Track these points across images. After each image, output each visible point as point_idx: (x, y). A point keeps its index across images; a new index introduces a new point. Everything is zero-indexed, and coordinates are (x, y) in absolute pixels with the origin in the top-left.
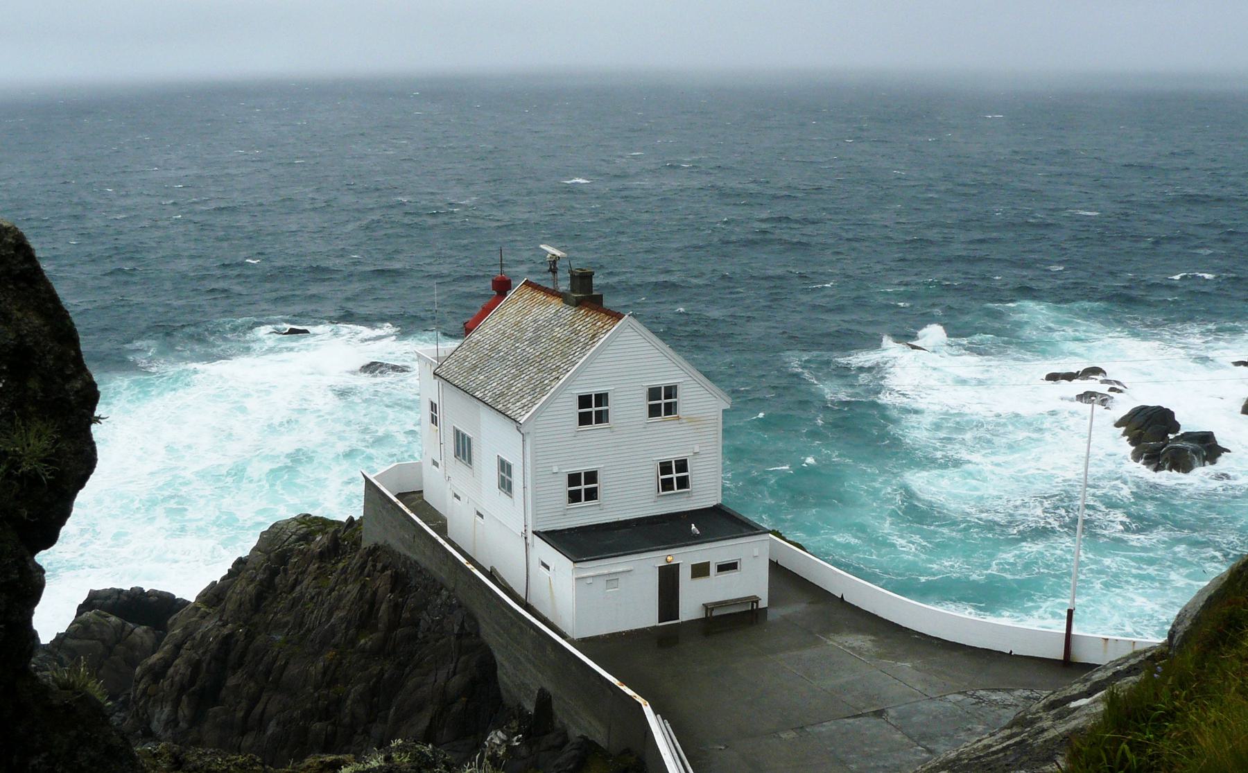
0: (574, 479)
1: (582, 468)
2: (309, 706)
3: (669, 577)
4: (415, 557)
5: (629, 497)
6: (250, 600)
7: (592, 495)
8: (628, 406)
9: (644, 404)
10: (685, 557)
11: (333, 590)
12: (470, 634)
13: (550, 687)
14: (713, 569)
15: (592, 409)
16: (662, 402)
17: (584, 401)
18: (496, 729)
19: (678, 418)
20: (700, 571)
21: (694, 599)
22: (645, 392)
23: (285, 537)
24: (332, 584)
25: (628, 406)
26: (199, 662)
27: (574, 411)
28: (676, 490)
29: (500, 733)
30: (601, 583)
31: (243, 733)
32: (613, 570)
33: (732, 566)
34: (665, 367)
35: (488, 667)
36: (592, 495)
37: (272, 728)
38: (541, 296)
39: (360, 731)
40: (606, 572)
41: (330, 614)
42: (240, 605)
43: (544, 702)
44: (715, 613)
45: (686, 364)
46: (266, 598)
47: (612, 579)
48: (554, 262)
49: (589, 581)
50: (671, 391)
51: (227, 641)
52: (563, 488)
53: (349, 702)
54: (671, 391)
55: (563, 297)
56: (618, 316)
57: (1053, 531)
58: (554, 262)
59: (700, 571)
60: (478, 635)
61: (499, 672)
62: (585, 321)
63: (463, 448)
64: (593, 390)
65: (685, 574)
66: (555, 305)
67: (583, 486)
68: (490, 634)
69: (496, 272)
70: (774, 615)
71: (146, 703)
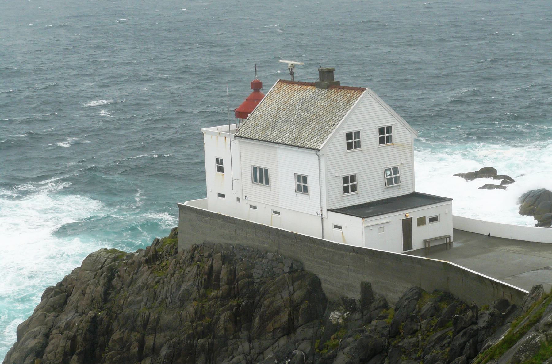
0: (345, 180)
1: (349, 173)
2: (191, 332)
3: (407, 224)
5: (371, 191)
6: (101, 296)
7: (354, 189)
8: (369, 138)
10: (414, 214)
11: (173, 274)
13: (368, 279)
14: (427, 220)
15: (353, 141)
16: (385, 135)
17: (349, 136)
18: (333, 311)
19: (393, 144)
20: (421, 222)
21: (420, 236)
22: (377, 130)
23: (103, 261)
24: (171, 271)
25: (369, 138)
26: (75, 337)
27: (344, 141)
28: (394, 185)
29: (336, 313)
30: (376, 229)
35: (316, 283)
36: (354, 189)
37: (164, 352)
38: (296, 87)
41: (179, 286)
42: (92, 301)
43: (366, 289)
44: (431, 245)
45: (396, 115)
46: (110, 294)
47: (381, 226)
49: (371, 228)
50: (389, 129)
51: (94, 321)
52: (340, 185)
53: (221, 323)
54: (389, 129)
56: (362, 90)
57: (440, 301)
59: (421, 222)
60: (303, 270)
61: (324, 285)
63: (261, 176)
64: (352, 130)
65: (414, 223)
66: (310, 91)
67: (349, 184)
68: (312, 266)
69: (253, 78)
70: (455, 245)
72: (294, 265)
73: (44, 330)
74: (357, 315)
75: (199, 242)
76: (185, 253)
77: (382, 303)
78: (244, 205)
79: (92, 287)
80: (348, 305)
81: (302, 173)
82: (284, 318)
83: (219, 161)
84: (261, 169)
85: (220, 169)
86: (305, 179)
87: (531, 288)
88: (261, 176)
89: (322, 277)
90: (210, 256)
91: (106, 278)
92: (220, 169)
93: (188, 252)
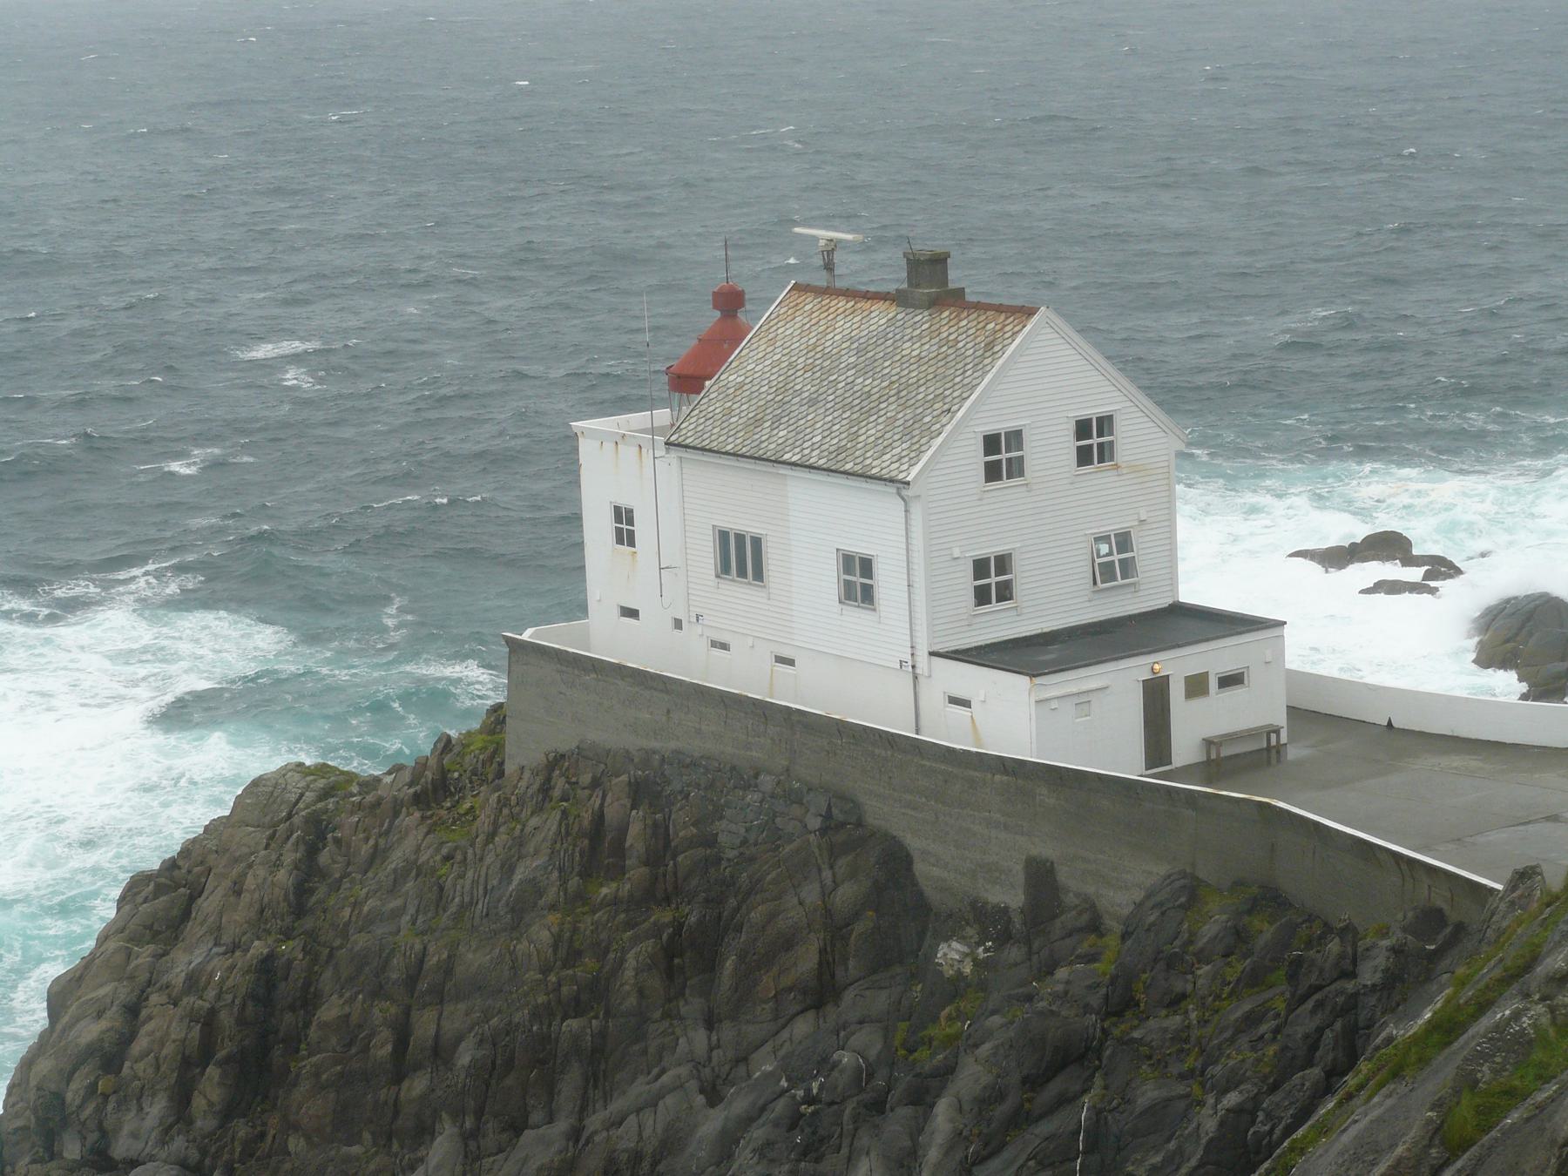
1: (990, 550)
2: (541, 999)
3: (1156, 694)
4: (673, 745)
5: (1053, 599)
7: (1005, 592)
8: (1048, 450)
9: (1070, 445)
10: (1176, 664)
12: (843, 825)
13: (1045, 849)
14: (1213, 683)
15: (1001, 457)
16: (1093, 441)
18: (947, 939)
19: (1117, 467)
20: (1197, 686)
21: (1192, 727)
22: (1072, 426)
23: (293, 798)
25: (1048, 450)
27: (977, 459)
28: (1120, 582)
29: (955, 945)
31: (398, 1078)
32: (1085, 688)
33: (1231, 681)
34: (1098, 389)
35: (897, 861)
36: (1005, 592)
38: (841, 304)
39: (657, 1015)
40: (1075, 690)
41: (508, 869)
43: (1041, 877)
44: (1226, 751)
45: (1125, 382)
46: (312, 891)
47: (1083, 700)
48: (830, 252)
49: (1054, 704)
50: (1105, 424)
51: (267, 968)
52: (966, 583)
53: (629, 973)
54: (1105, 424)
55: (899, 299)
56: (1030, 312)
58: (830, 252)
59: (1197, 686)
60: (859, 824)
61: (919, 867)
62: (920, 335)
66: (880, 316)
67: (992, 580)
68: (885, 812)
69: (719, 280)
70: (1292, 753)
71: (100, 1110)
72: (835, 811)
73: (124, 993)
74: (1014, 953)
75: (566, 743)
76: (527, 775)
77: (1085, 917)
78: (694, 641)
79: (262, 872)
80: (988, 921)
81: (860, 548)
82: (805, 961)
83: (623, 516)
84: (740, 538)
85: (625, 537)
86: (866, 566)
87: (1508, 875)
88: (741, 557)
89: (913, 843)
90: (596, 783)
91: (302, 848)
92: (625, 537)
93: (535, 773)
